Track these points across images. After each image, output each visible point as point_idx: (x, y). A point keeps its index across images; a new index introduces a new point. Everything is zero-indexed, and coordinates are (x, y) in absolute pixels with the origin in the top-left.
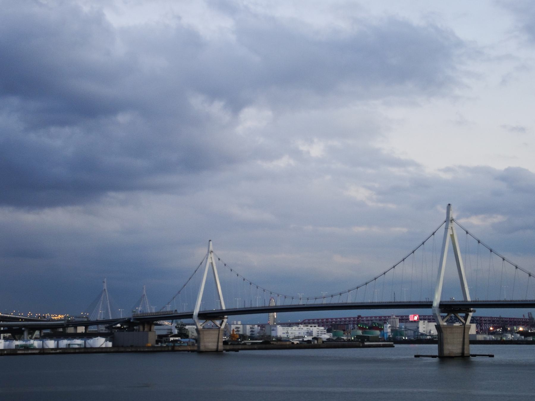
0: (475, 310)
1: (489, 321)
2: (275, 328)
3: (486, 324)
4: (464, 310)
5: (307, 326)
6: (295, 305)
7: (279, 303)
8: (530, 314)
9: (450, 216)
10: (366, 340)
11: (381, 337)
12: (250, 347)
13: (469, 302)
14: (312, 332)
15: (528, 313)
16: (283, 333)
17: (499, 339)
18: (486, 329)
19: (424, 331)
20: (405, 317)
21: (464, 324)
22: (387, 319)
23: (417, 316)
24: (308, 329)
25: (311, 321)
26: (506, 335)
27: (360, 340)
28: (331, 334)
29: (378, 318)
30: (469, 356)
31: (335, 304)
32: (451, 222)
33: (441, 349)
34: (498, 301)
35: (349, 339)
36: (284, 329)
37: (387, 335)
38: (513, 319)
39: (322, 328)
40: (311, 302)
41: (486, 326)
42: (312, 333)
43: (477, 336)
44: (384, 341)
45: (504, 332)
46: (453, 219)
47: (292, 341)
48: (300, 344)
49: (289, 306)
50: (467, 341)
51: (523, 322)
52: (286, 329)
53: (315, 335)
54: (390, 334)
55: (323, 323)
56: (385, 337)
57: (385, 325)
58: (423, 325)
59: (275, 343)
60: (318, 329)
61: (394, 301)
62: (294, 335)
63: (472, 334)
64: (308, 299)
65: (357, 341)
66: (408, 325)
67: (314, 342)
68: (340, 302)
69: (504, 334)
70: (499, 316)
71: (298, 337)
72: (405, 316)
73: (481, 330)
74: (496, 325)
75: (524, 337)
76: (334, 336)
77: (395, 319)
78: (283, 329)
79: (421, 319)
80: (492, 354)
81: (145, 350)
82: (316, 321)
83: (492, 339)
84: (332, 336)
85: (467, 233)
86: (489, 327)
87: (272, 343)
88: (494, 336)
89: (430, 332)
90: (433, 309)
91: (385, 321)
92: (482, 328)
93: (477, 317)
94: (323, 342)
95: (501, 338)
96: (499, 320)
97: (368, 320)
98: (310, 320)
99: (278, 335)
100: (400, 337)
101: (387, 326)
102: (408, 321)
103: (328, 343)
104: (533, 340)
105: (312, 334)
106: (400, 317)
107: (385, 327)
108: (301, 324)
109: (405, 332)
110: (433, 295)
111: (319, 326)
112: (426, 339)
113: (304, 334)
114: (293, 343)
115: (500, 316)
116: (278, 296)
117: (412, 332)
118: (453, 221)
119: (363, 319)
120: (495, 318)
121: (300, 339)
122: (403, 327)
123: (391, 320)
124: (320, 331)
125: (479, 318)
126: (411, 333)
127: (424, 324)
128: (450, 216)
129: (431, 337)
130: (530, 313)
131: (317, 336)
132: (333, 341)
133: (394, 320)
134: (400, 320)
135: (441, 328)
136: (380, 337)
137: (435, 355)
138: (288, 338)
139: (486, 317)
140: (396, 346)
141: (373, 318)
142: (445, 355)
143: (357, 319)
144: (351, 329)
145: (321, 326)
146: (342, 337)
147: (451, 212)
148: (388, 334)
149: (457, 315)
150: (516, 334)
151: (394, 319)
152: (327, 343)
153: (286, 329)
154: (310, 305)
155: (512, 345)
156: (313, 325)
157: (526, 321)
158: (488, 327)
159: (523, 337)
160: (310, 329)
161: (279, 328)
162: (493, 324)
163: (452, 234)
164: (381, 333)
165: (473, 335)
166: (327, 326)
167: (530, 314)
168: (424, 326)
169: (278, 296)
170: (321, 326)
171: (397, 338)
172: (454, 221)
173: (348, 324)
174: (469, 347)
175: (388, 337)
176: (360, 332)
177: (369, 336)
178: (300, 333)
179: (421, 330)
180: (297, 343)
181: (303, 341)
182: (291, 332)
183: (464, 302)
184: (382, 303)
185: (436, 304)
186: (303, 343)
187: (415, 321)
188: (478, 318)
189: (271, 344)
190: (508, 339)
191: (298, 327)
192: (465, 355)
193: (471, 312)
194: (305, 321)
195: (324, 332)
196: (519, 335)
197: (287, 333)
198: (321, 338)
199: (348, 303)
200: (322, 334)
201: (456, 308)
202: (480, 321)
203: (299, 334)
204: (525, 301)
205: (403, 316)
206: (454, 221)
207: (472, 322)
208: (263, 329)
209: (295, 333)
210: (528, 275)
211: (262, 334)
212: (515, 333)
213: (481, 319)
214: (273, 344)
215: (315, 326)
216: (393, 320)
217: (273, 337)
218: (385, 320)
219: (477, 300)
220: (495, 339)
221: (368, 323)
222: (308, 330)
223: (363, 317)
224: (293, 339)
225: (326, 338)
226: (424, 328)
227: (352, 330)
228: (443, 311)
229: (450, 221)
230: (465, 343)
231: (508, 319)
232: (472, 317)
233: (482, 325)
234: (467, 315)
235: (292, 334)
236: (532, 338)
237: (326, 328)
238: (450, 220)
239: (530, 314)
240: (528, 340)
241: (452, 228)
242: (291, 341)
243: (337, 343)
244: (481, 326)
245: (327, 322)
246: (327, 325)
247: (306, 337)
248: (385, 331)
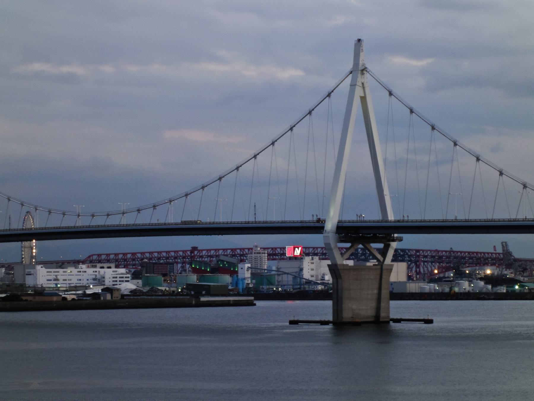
0: (402, 237)
1: (433, 257)
2: (32, 271)
3: (426, 264)
4: (382, 238)
5: (95, 267)
6: (69, 227)
8: (504, 245)
9: (361, 62)
10: (204, 292)
11: (232, 286)
13: (390, 222)
14: (104, 278)
15: (502, 243)
16: (48, 280)
17: (447, 290)
18: (426, 272)
19: (312, 276)
20: (279, 250)
21: (381, 264)
22: (246, 254)
23: (300, 248)
24: (96, 272)
25: (103, 257)
26: (459, 284)
27: (193, 293)
28: (140, 281)
29: (229, 251)
30: (388, 322)
31: (143, 225)
32: (363, 74)
33: (337, 310)
34: (421, 221)
35: (173, 291)
36: (51, 272)
37: (243, 283)
38: (475, 254)
39: (123, 270)
41: (426, 267)
42: (103, 280)
43: (408, 284)
44: (238, 295)
45: (457, 278)
46: (366, 68)
47: (63, 296)
48: (79, 300)
49: (57, 228)
50: (385, 293)
51: (493, 259)
52: (54, 272)
53: (108, 283)
54: (249, 282)
55: (125, 260)
56: (241, 287)
57: (240, 266)
58: (310, 264)
59: (30, 298)
60: (114, 273)
61: (254, 220)
62: (70, 284)
63: (399, 281)
64: (93, 216)
65: (187, 295)
66: (284, 265)
67: (105, 297)
68: (154, 221)
69: (456, 282)
70: (448, 249)
71: (76, 288)
72: (246, 249)
73: (418, 273)
74: (444, 265)
75: (492, 288)
76: (144, 285)
77: (260, 253)
78: (48, 272)
79: (308, 255)
80: (430, 318)
82: (112, 257)
83: (435, 290)
84: (141, 286)
85: (391, 94)
86: (432, 269)
87: (24, 298)
88: (438, 284)
89: (323, 279)
90: (325, 235)
91: (242, 258)
92: (420, 270)
93: (411, 250)
94: (123, 296)
95: (451, 289)
96: (450, 256)
97: (211, 256)
98: (109, 254)
99: (38, 283)
100: (268, 287)
101: (245, 267)
102: (285, 257)
103: (132, 297)
104: (507, 291)
105: (104, 281)
106: (269, 250)
107: (240, 269)
108: (84, 262)
109: (276, 276)
110: (326, 209)
111: (117, 267)
112: (314, 291)
113: (88, 282)
114: (65, 299)
115: (451, 248)
116: (36, 209)
117: (290, 278)
118: (365, 72)
119: (201, 254)
120: (442, 251)
121: (77, 291)
122: (274, 268)
123: (253, 255)
124: (118, 276)
125: (414, 251)
126: (288, 280)
127: (313, 263)
128: (361, 62)
129: (325, 286)
130: (506, 243)
131: (114, 285)
132: (143, 295)
133: (258, 255)
134: (269, 255)
135: (338, 270)
136: (230, 287)
137: (326, 320)
138: (58, 289)
139: (427, 251)
140: (259, 303)
141: (221, 252)
142: (344, 320)
143: (189, 254)
144: (179, 272)
145: (123, 266)
146: (160, 288)
147: (362, 54)
148: (246, 282)
149: (369, 247)
150: (479, 281)
151: (258, 253)
152: (131, 299)
153: (54, 272)
154: (96, 226)
155: (513, 301)
156: (106, 265)
157: (498, 258)
158: (430, 269)
159: (490, 287)
160: (99, 271)
161: (41, 271)
162: (439, 263)
163: (363, 95)
164: (233, 279)
165: (403, 282)
166: (134, 267)
167: (504, 244)
168: (313, 266)
169: (36, 209)
170: (123, 266)
171: (263, 288)
172: (368, 72)
173: (172, 264)
174: (389, 305)
175: (245, 287)
176: (193, 279)
177: (210, 285)
178: (80, 280)
179: (307, 274)
180: (73, 299)
181: (85, 295)
182: (64, 277)
183: (381, 222)
184: (231, 223)
185: (330, 225)
186: (84, 298)
187: (295, 258)
188: (413, 253)
189: (22, 300)
190: (462, 291)
191: (76, 268)
192: (381, 320)
193: (394, 240)
194: (91, 258)
195: (126, 277)
196: (482, 283)
197: (56, 280)
198: (118, 290)
199: (169, 224)
200: (123, 281)
201: (367, 234)
202: (416, 257)
203: (79, 282)
204: (492, 221)
205: (276, 248)
206: (366, 71)
207: (395, 259)
208: (10, 272)
209: (70, 280)
210: (498, 173)
211: (7, 283)
212: (477, 280)
213: (418, 254)
214: (26, 300)
215: (109, 267)
216: (256, 255)
217: (29, 287)
218: (241, 255)
219: (406, 218)
220: (441, 291)
221: (211, 261)
222: (96, 273)
223: (202, 250)
224: (67, 291)
225: (129, 289)
226: (312, 270)
227: (180, 273)
228: (342, 239)
229: (360, 72)
230: (382, 297)
231: (467, 254)
232: (396, 250)
233: (420, 264)
234: (387, 247)
235: (65, 282)
236: (505, 288)
237: (131, 270)
238: (360, 69)
239: (504, 244)
240: (499, 291)
241: (363, 84)
242: (61, 295)
243: (149, 297)
244: (418, 266)
245: (134, 260)
246: (133, 265)
247: (91, 286)
248: (240, 276)
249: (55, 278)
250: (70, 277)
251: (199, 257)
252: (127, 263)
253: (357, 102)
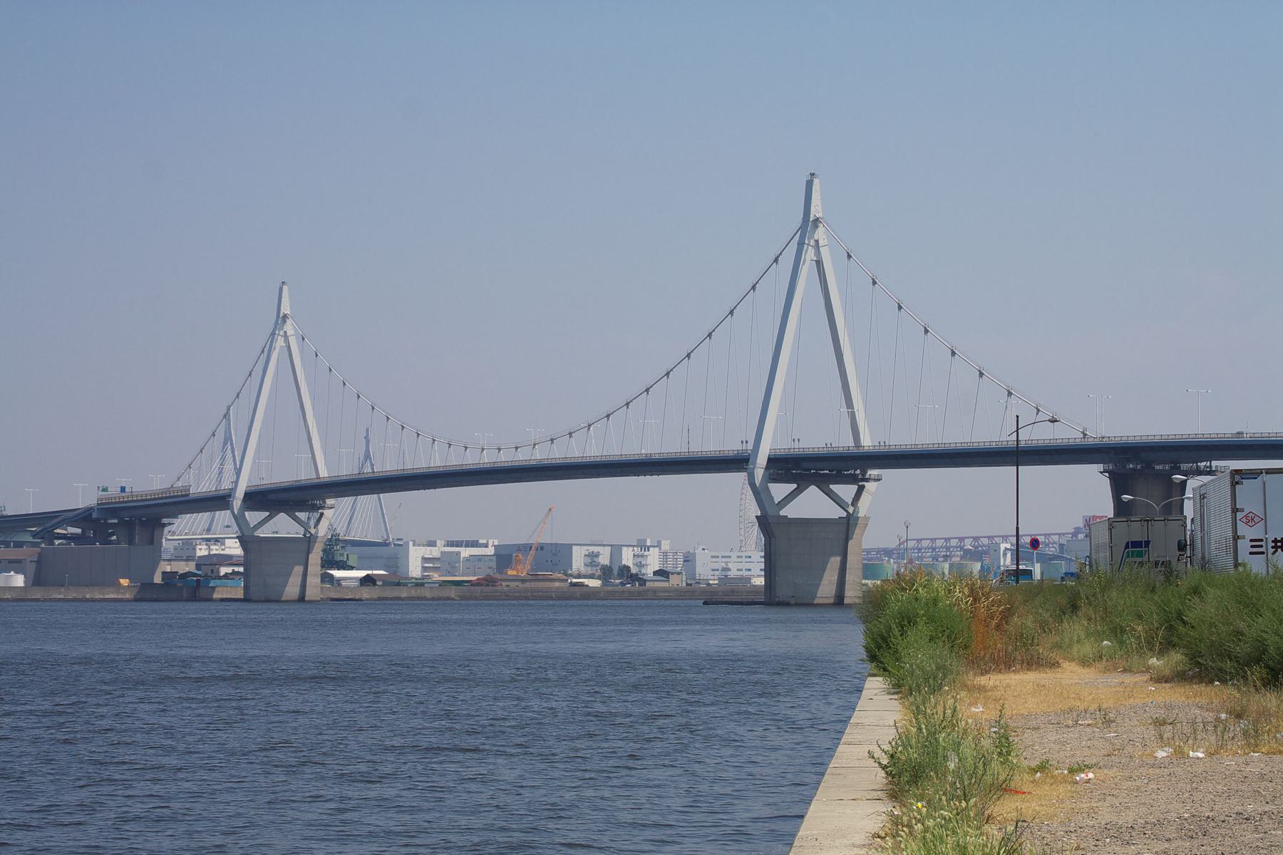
40: (506, 458)
81: (107, 596)
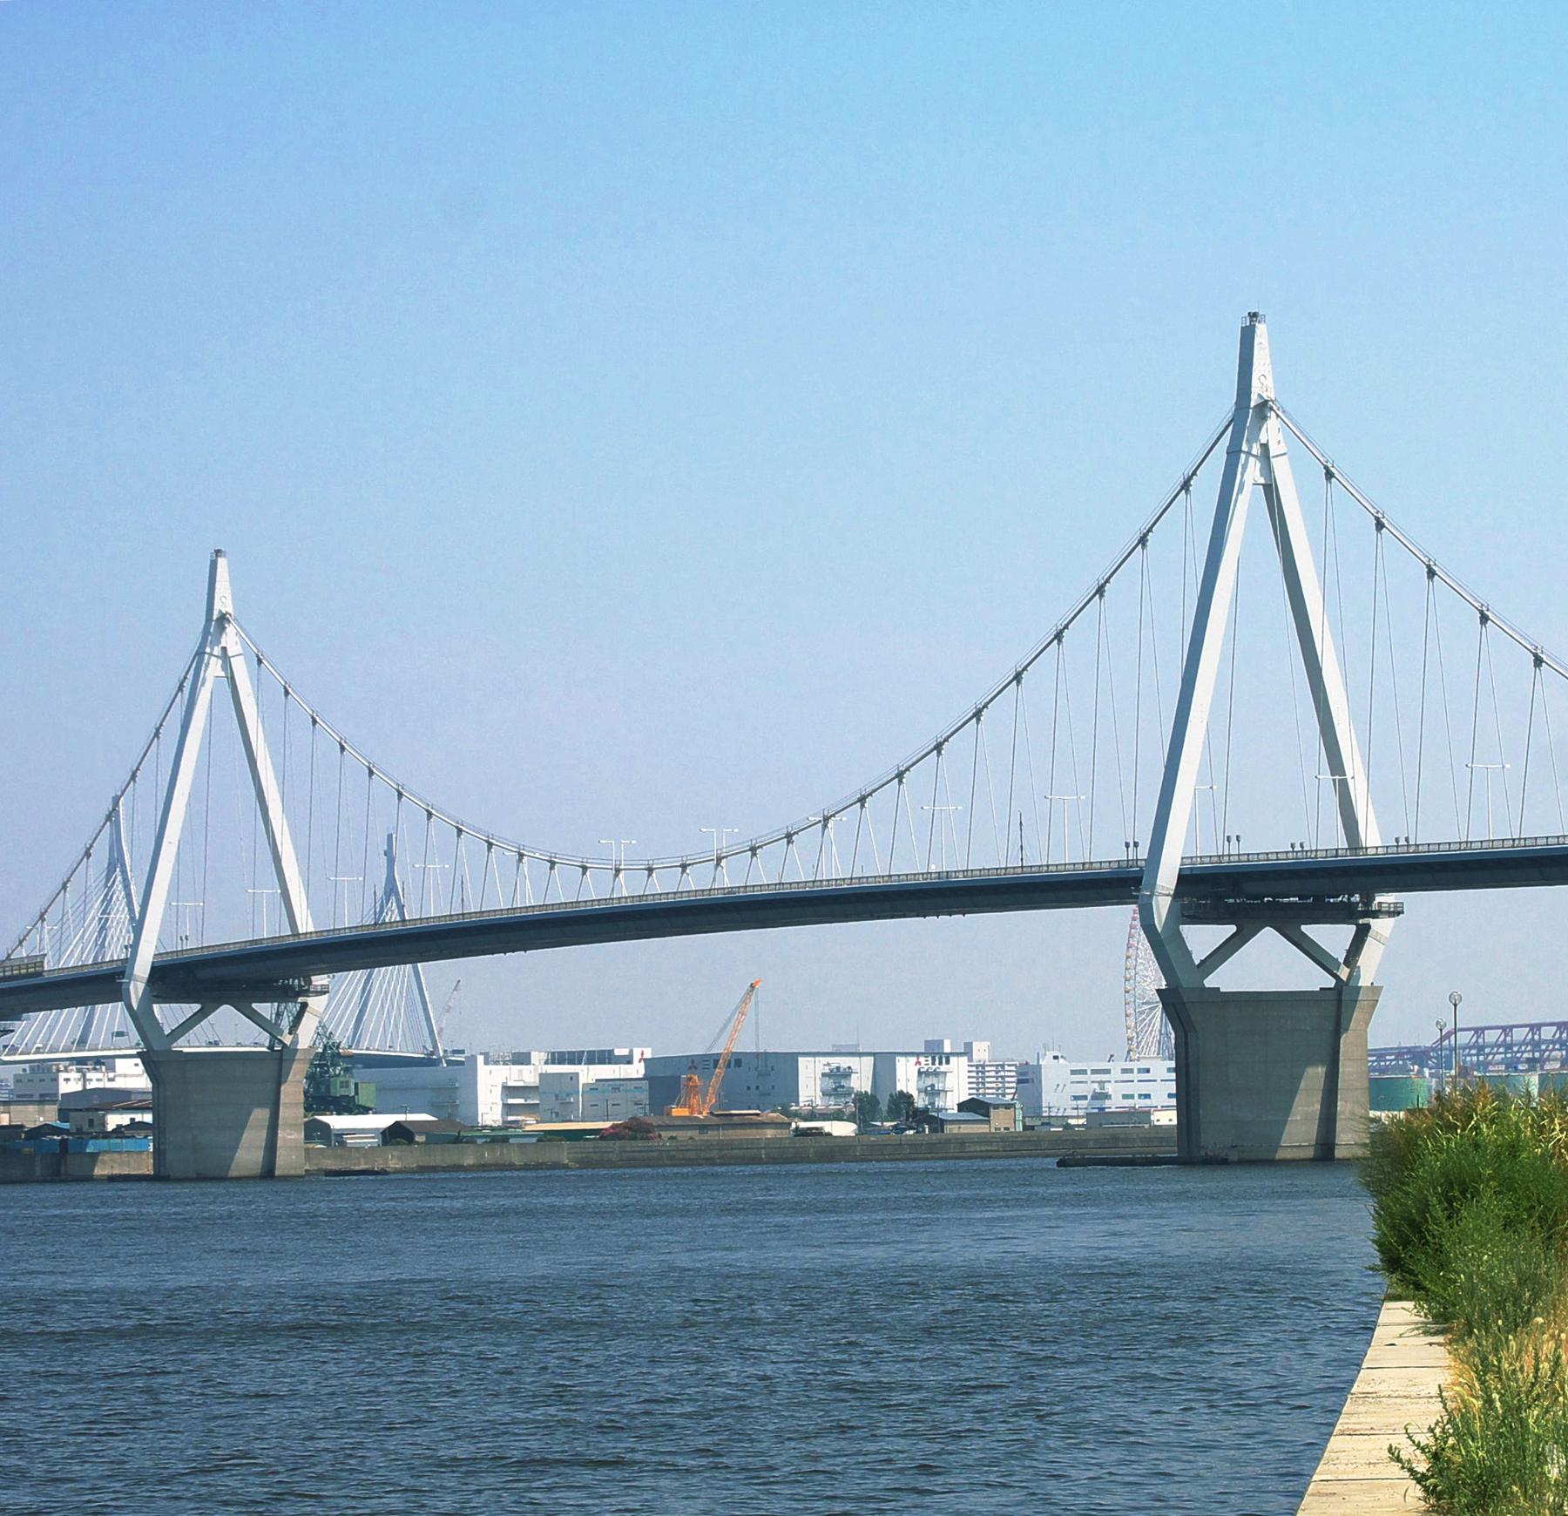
7: (70, 873)
12: (534, 1156)
53: (834, 1066)
98: (1483, 1029)
209: (1147, 1096)
249: (1098, 1091)
250: (1144, 1088)
251: (1557, 1046)
252: (1485, 1059)
253: (1247, 502)
